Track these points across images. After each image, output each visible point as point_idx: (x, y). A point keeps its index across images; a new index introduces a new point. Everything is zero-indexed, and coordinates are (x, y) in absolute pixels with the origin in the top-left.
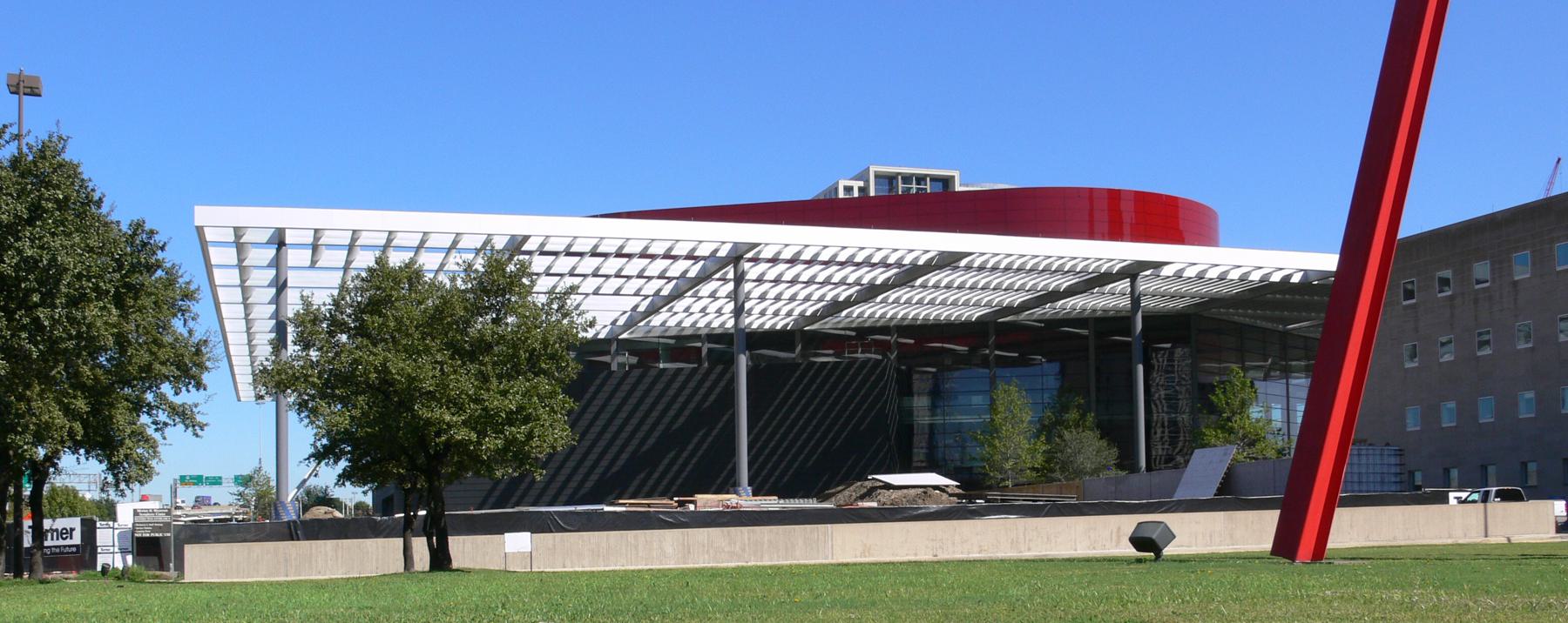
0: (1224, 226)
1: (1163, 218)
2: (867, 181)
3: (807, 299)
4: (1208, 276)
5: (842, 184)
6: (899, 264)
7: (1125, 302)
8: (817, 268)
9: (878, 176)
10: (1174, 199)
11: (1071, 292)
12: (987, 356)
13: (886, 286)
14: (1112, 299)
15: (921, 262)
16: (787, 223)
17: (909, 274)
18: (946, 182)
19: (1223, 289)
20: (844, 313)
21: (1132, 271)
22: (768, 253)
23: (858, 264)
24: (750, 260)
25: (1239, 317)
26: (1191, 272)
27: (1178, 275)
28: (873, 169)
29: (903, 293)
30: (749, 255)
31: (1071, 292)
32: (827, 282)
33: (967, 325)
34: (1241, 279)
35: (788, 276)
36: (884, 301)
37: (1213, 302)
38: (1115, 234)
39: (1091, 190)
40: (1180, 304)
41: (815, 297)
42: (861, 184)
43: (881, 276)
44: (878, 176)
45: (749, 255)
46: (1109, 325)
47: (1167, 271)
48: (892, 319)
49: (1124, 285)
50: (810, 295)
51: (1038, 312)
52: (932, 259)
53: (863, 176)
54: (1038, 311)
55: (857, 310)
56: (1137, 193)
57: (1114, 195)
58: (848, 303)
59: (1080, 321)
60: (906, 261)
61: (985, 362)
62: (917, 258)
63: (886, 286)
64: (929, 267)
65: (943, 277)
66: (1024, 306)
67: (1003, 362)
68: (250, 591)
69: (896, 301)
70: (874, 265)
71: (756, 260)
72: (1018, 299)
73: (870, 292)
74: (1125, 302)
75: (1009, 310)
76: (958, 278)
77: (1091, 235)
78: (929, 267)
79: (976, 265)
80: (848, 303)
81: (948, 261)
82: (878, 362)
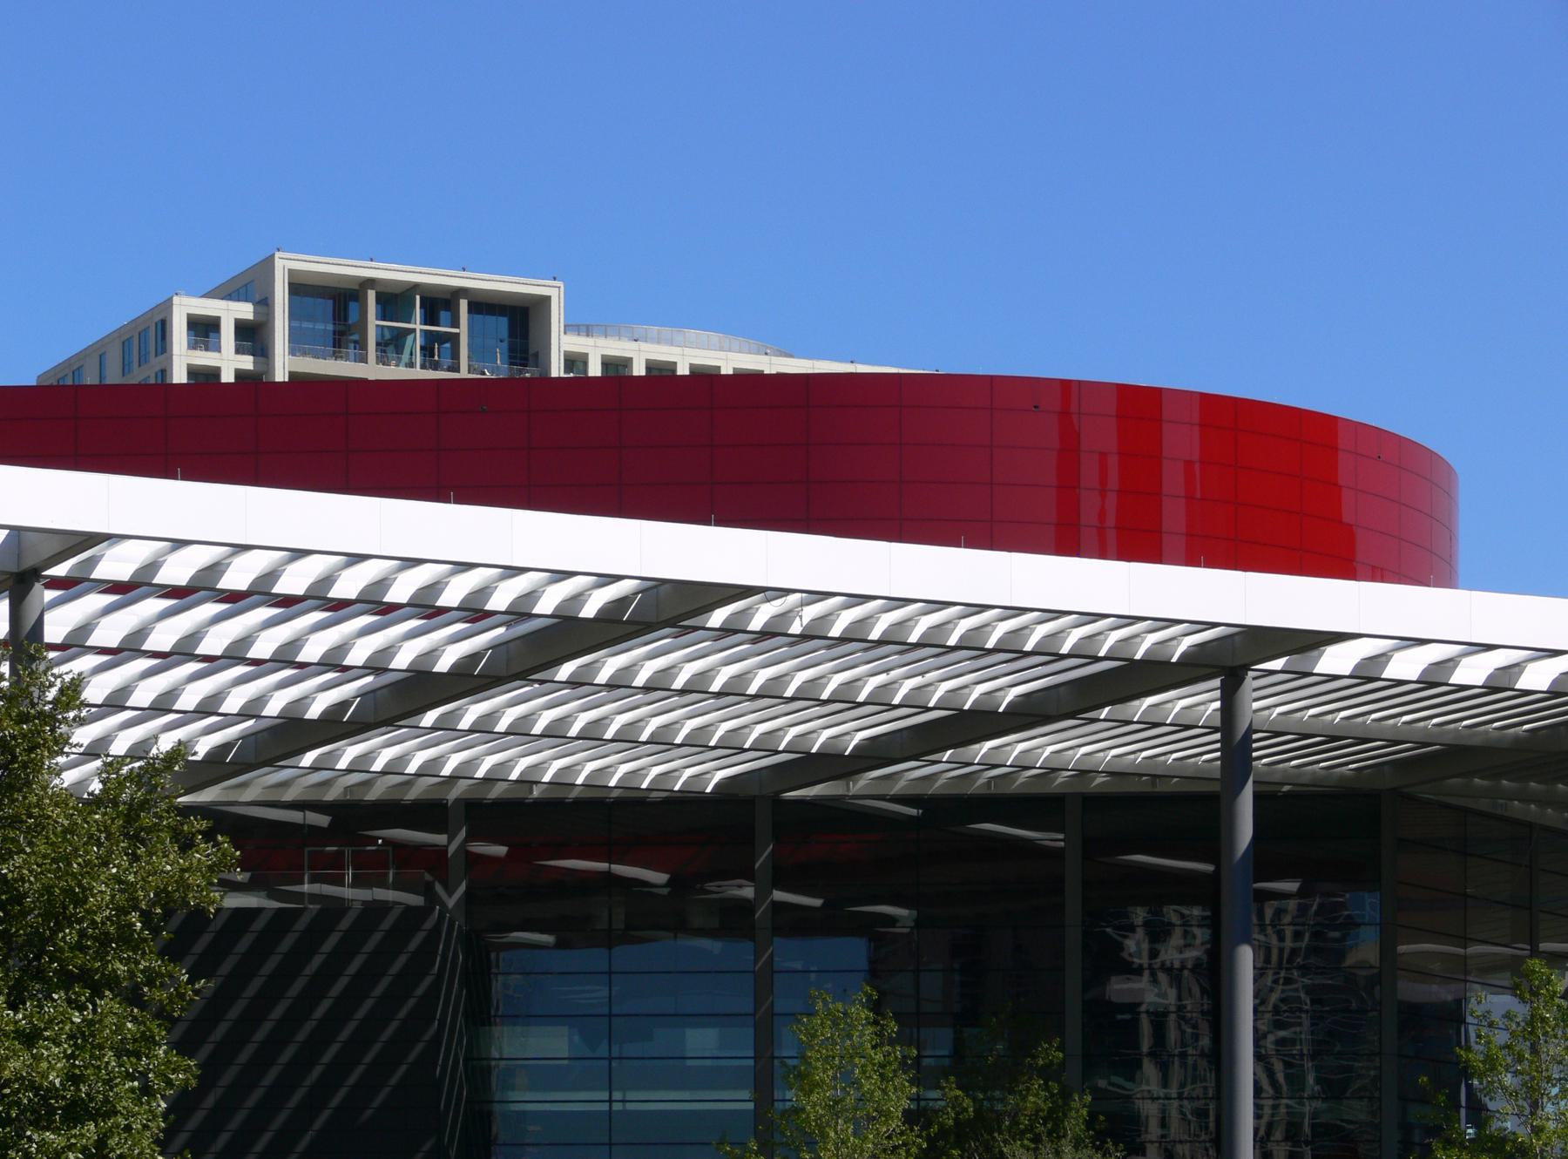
0: (1473, 522)
1: (1294, 487)
2: (264, 303)
3: (161, 706)
4: (1392, 671)
5: (184, 307)
6: (519, 612)
7: (1206, 754)
8: (152, 606)
9: (300, 288)
10: (1327, 423)
11: (1027, 715)
12: (745, 907)
13: (469, 680)
14: (1166, 734)
15: (589, 611)
16: (971, 544)
17: (543, 645)
18: (521, 321)
19: (1493, 723)
20: (309, 758)
21: (1231, 657)
22: (116, 564)
23: (287, 601)
24: (55, 583)
25: (1525, 802)
26: (1407, 666)
27: (1367, 673)
28: (284, 265)
29: (504, 707)
30: (61, 570)
31: (1027, 715)
32: (184, 651)
33: (689, 803)
34: (1491, 688)
35: (163, 638)
36: (446, 726)
37: (1458, 756)
38: (1139, 542)
39: (1066, 387)
40: (1346, 763)
41: (232, 704)
42: (246, 311)
43: (451, 650)
44: (300, 288)
45: (61, 570)
46: (1163, 813)
47: (1336, 661)
48: (488, 780)
49: (1203, 700)
50: (170, 695)
51: (911, 772)
52: (622, 602)
53: (253, 285)
54: (911, 772)
55: (350, 752)
56: (1123, 390)
57: (1139, 407)
58: (335, 727)
59: (1038, 802)
60: (547, 604)
61: (734, 921)
62: (578, 598)
63: (469, 680)
64: (616, 627)
65: (642, 660)
66: (875, 753)
67: (793, 923)
68: (1264, 1028)
69: (483, 728)
70: (340, 605)
71: (71, 586)
72: (856, 734)
73: (405, 697)
74: (1206, 754)
75: (831, 763)
76: (684, 662)
77: (1067, 543)
78: (616, 627)
79: (756, 624)
80: (335, 727)
81: (672, 607)
82: (412, 917)
